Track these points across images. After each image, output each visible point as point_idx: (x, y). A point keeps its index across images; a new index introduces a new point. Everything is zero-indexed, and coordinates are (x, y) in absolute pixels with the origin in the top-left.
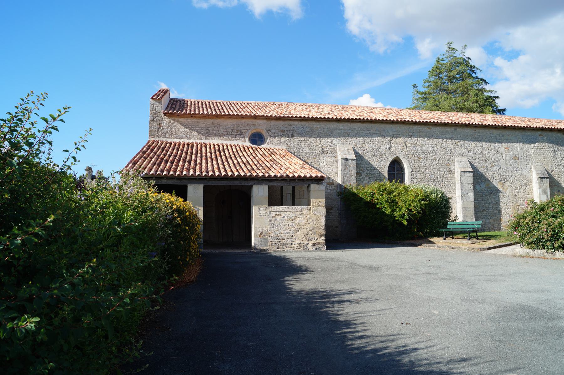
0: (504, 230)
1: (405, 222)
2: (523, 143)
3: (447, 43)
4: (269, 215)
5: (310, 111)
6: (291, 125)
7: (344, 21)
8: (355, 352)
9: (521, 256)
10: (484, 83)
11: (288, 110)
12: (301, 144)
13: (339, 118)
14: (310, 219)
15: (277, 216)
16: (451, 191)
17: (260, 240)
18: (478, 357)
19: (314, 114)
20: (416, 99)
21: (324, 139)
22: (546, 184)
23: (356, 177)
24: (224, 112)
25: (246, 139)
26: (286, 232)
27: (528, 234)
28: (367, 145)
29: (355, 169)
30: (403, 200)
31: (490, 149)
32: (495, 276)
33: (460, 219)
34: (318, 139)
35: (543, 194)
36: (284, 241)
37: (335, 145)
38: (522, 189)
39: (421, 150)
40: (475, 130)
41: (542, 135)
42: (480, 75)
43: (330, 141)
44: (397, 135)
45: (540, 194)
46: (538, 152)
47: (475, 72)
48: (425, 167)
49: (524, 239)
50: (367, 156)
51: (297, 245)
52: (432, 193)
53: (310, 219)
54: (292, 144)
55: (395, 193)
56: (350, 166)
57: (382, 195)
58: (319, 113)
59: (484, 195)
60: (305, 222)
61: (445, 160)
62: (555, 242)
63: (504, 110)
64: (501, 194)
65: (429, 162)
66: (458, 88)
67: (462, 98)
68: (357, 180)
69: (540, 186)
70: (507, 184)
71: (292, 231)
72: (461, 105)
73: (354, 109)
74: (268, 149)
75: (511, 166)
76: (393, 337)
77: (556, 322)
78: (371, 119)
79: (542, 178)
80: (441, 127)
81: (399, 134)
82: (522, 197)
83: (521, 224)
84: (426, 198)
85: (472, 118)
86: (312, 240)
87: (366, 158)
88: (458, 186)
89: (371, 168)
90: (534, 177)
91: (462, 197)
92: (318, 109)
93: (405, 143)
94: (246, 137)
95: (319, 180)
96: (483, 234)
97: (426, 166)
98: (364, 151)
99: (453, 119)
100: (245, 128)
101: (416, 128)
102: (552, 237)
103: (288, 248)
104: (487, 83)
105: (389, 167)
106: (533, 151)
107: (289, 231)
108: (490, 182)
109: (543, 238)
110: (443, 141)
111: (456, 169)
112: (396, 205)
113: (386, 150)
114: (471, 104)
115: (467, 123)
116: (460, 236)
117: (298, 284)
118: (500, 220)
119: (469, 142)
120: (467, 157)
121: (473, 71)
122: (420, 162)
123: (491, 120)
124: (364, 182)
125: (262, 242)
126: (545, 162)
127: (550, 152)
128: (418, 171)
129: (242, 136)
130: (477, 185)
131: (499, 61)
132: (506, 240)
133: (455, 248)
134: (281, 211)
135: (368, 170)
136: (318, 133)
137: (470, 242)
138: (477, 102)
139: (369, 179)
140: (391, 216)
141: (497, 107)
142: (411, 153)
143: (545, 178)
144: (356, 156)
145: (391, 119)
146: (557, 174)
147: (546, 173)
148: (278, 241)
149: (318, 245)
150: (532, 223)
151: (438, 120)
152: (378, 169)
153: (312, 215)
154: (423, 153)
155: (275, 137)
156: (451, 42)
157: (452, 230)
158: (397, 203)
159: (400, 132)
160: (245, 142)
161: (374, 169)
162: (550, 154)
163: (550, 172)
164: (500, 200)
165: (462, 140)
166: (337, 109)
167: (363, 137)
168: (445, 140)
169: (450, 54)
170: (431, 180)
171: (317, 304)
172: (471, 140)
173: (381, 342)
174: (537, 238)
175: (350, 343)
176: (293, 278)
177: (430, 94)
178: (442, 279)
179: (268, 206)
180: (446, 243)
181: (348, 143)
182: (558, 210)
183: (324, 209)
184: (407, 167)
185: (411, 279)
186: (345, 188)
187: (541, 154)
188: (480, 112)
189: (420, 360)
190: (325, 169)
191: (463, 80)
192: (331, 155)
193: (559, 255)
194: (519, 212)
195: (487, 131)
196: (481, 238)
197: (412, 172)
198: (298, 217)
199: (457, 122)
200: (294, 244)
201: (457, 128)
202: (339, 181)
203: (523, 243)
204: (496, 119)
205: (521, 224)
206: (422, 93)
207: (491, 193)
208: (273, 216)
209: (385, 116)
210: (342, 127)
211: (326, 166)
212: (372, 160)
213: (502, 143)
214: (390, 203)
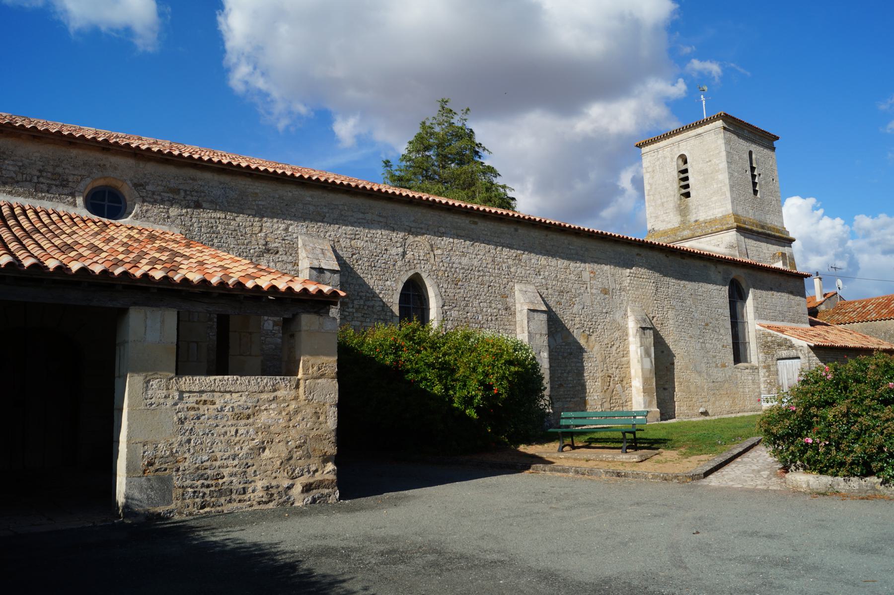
1: (471, 412)
2: (615, 266)
3: (440, 100)
4: (176, 404)
6: (194, 179)
7: (224, 72)
14: (296, 412)
15: (200, 406)
17: (145, 484)
21: (270, 220)
22: (650, 339)
25: (77, 199)
26: (227, 454)
28: (360, 244)
31: (568, 271)
34: (257, 219)
35: (645, 357)
36: (221, 481)
37: (295, 235)
38: (614, 348)
39: (460, 263)
40: (547, 236)
43: (283, 226)
45: (641, 356)
46: (635, 283)
47: (480, 154)
48: (466, 299)
50: (360, 267)
51: (260, 493)
52: (515, 350)
53: (296, 412)
54: (195, 225)
59: (560, 358)
60: (282, 422)
61: (499, 287)
64: (585, 355)
65: (473, 289)
69: (641, 343)
70: (593, 338)
71: (246, 449)
79: (643, 329)
80: (492, 223)
82: (615, 361)
86: (302, 475)
89: (368, 295)
90: (632, 325)
93: (431, 246)
97: (468, 296)
98: (354, 257)
100: (76, 172)
103: (235, 505)
105: (401, 294)
107: (237, 452)
108: (570, 333)
110: (495, 249)
113: (397, 257)
119: (538, 256)
120: (534, 284)
121: (477, 153)
125: (152, 489)
126: (644, 301)
127: (651, 284)
128: (454, 305)
129: (66, 191)
134: (214, 391)
135: (361, 298)
136: (258, 205)
139: (363, 316)
140: (445, 401)
142: (443, 268)
144: (339, 265)
146: (660, 323)
148: (203, 485)
149: (317, 487)
152: (381, 296)
153: (303, 403)
155: (154, 202)
159: (421, 223)
160: (75, 205)
161: (374, 296)
162: (651, 288)
163: (651, 319)
164: (583, 367)
165: (527, 251)
167: (352, 226)
168: (499, 248)
169: (444, 118)
170: (477, 325)
172: (541, 253)
179: (173, 375)
181: (322, 235)
183: (335, 384)
184: (436, 296)
187: (639, 287)
192: (285, 258)
197: (443, 306)
198: (263, 408)
200: (250, 490)
201: (519, 227)
207: (571, 354)
208: (190, 405)
210: (310, 199)
212: (369, 276)
213: (585, 262)
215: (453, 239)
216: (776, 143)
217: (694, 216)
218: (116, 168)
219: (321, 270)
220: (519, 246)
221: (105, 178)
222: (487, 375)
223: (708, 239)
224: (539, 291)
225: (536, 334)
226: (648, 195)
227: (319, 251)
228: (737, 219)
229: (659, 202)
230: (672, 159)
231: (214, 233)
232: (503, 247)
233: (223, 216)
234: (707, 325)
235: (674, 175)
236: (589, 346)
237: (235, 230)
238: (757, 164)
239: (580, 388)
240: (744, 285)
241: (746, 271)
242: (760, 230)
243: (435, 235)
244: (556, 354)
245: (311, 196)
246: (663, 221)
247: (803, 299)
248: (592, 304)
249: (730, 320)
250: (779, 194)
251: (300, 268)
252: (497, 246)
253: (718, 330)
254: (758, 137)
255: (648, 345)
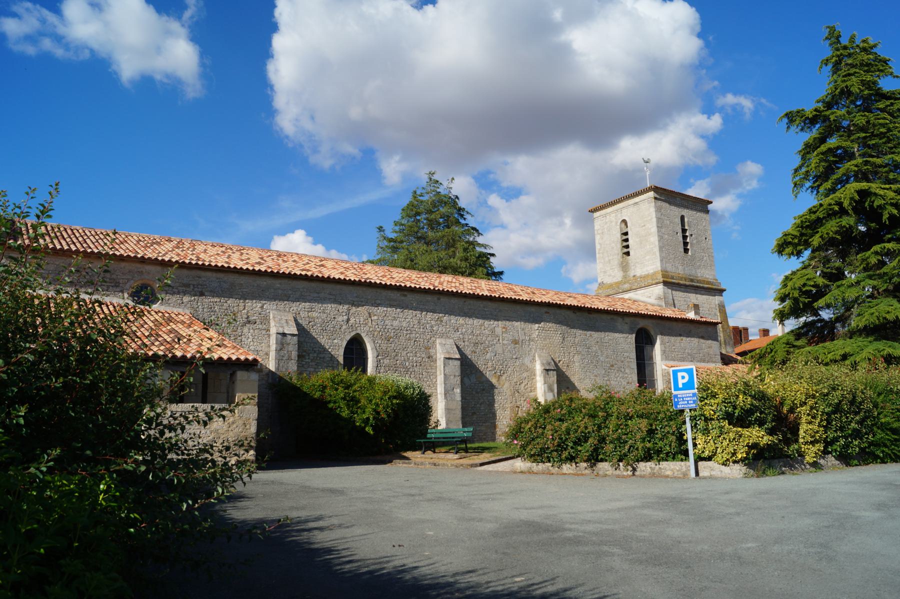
0: (501, 439)
1: (369, 430)
2: (525, 322)
3: (428, 173)
5: (229, 257)
6: (200, 277)
8: (348, 575)
9: (522, 472)
10: (476, 235)
11: (194, 252)
12: (214, 308)
13: (275, 271)
14: (233, 423)
16: (431, 385)
18: (483, 569)
19: (236, 262)
20: (382, 248)
23: (298, 361)
24: (90, 248)
27: (530, 443)
28: (315, 314)
29: (297, 349)
30: (367, 397)
31: (483, 328)
32: (493, 494)
33: (443, 426)
34: (242, 301)
35: (548, 392)
37: (268, 311)
38: (523, 385)
39: (392, 325)
41: (548, 313)
42: (471, 221)
43: (260, 305)
44: (358, 301)
45: (545, 391)
47: (465, 217)
49: (525, 450)
52: (406, 388)
53: (233, 423)
54: (200, 307)
55: (356, 387)
56: (288, 344)
57: (337, 390)
58: (245, 262)
59: (474, 393)
60: (225, 428)
61: (424, 341)
62: (562, 452)
63: (501, 273)
65: (402, 343)
66: (444, 236)
67: (446, 252)
68: (298, 366)
70: (504, 378)
72: (445, 262)
73: (296, 258)
74: (162, 313)
75: (509, 353)
76: (387, 559)
77: (561, 533)
78: (323, 277)
79: (547, 370)
81: (362, 302)
83: (522, 430)
84: (399, 395)
85: (460, 284)
87: (313, 334)
88: (440, 379)
90: (538, 368)
91: (445, 394)
92: (242, 254)
93: (369, 314)
94: (125, 291)
95: (251, 365)
96: (476, 445)
98: (310, 324)
99: (436, 284)
101: (385, 293)
102: (559, 445)
104: (479, 234)
105: (346, 348)
106: (537, 334)
108: (483, 374)
109: (548, 448)
111: (438, 355)
112: (356, 404)
114: (459, 262)
115: (455, 291)
116: (444, 449)
117: (239, 514)
118: (494, 426)
121: (462, 216)
122: (390, 342)
123: (485, 289)
124: (309, 369)
126: (551, 348)
129: (118, 290)
130: (465, 378)
131: (494, 200)
132: (504, 452)
133: (438, 465)
135: (315, 352)
136: (242, 292)
137: (457, 456)
138: (466, 259)
140: (350, 421)
141: (492, 268)
142: (378, 329)
143: (551, 370)
145: (351, 278)
147: (553, 363)
150: (536, 428)
151: (415, 284)
152: (330, 350)
154: (394, 331)
156: (433, 171)
157: (433, 440)
158: (358, 401)
162: (558, 338)
163: (557, 362)
166: (270, 256)
168: (424, 313)
169: (432, 188)
171: (278, 534)
172: (459, 315)
173: (375, 564)
174: (541, 449)
175: (339, 567)
176: (227, 507)
177: (402, 242)
178: (429, 500)
180: (425, 458)
181: (287, 310)
182: (565, 412)
183: (256, 408)
184: (372, 349)
185: (390, 502)
186: (281, 378)
188: (470, 275)
189: (423, 576)
190: (251, 348)
191: (448, 227)
192: (260, 326)
193: (567, 470)
194: (520, 414)
195: (480, 304)
196: (472, 451)
197: (378, 356)
199: (441, 289)
201: (441, 297)
202: (272, 366)
203: (524, 455)
204: (491, 287)
205: (522, 430)
206: (391, 240)
207: (484, 390)
209: (342, 273)
210: (279, 286)
211: (252, 343)
212: (322, 337)
213: (498, 321)
214: (348, 401)
215: (387, 307)
216: (710, 207)
217: (633, 271)
218: (149, 273)
219: (284, 335)
220: (441, 310)
221: (142, 279)
222: (377, 405)
223: (642, 291)
224: (457, 343)
225: (450, 375)
226: (599, 253)
227: (283, 322)
228: (664, 276)
229: (607, 259)
230: (616, 223)
231: (212, 311)
232: (428, 312)
233: (219, 300)
234: (612, 366)
235: (618, 237)
236: (499, 384)
237: (227, 309)
238: (689, 226)
239: (491, 416)
240: (652, 333)
241: (654, 321)
242: (688, 283)
243: (372, 306)
244: (470, 390)
245: (280, 284)
246: (610, 276)
247: (715, 342)
248: (503, 352)
249: (635, 361)
250: (712, 251)
251: (271, 333)
252: (422, 311)
253: (623, 370)
254: (690, 203)
255: (551, 383)
